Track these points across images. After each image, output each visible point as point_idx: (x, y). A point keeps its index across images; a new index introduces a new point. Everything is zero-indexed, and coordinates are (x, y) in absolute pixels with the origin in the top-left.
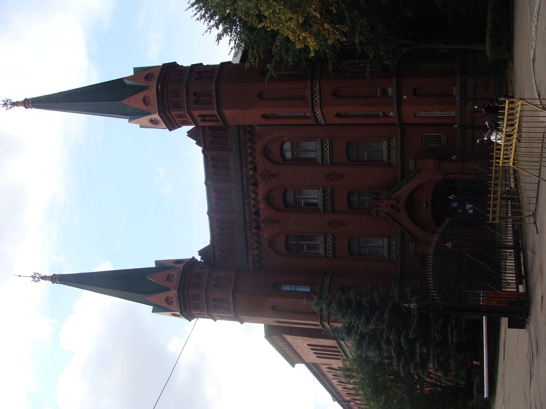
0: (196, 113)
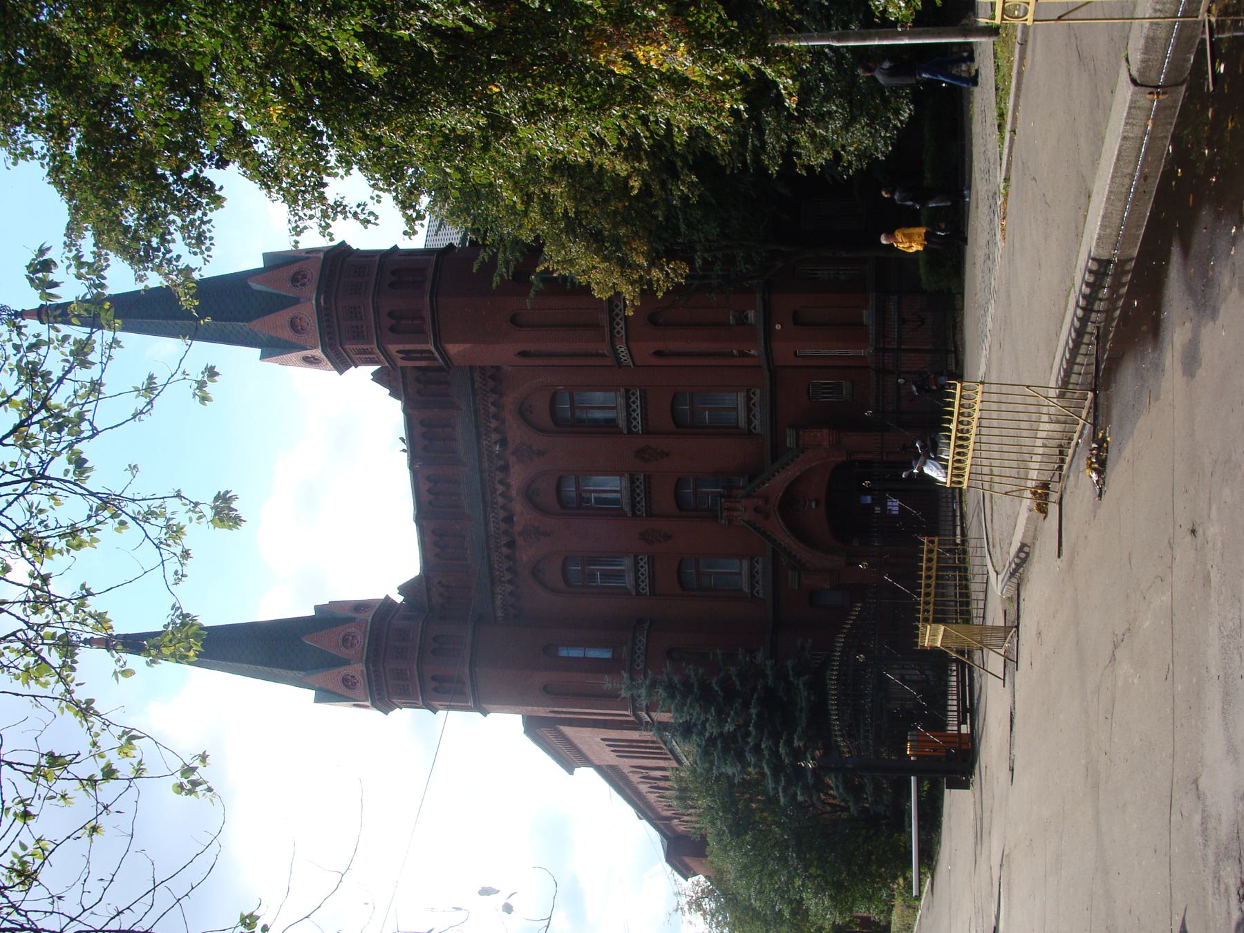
0: (393, 348)
